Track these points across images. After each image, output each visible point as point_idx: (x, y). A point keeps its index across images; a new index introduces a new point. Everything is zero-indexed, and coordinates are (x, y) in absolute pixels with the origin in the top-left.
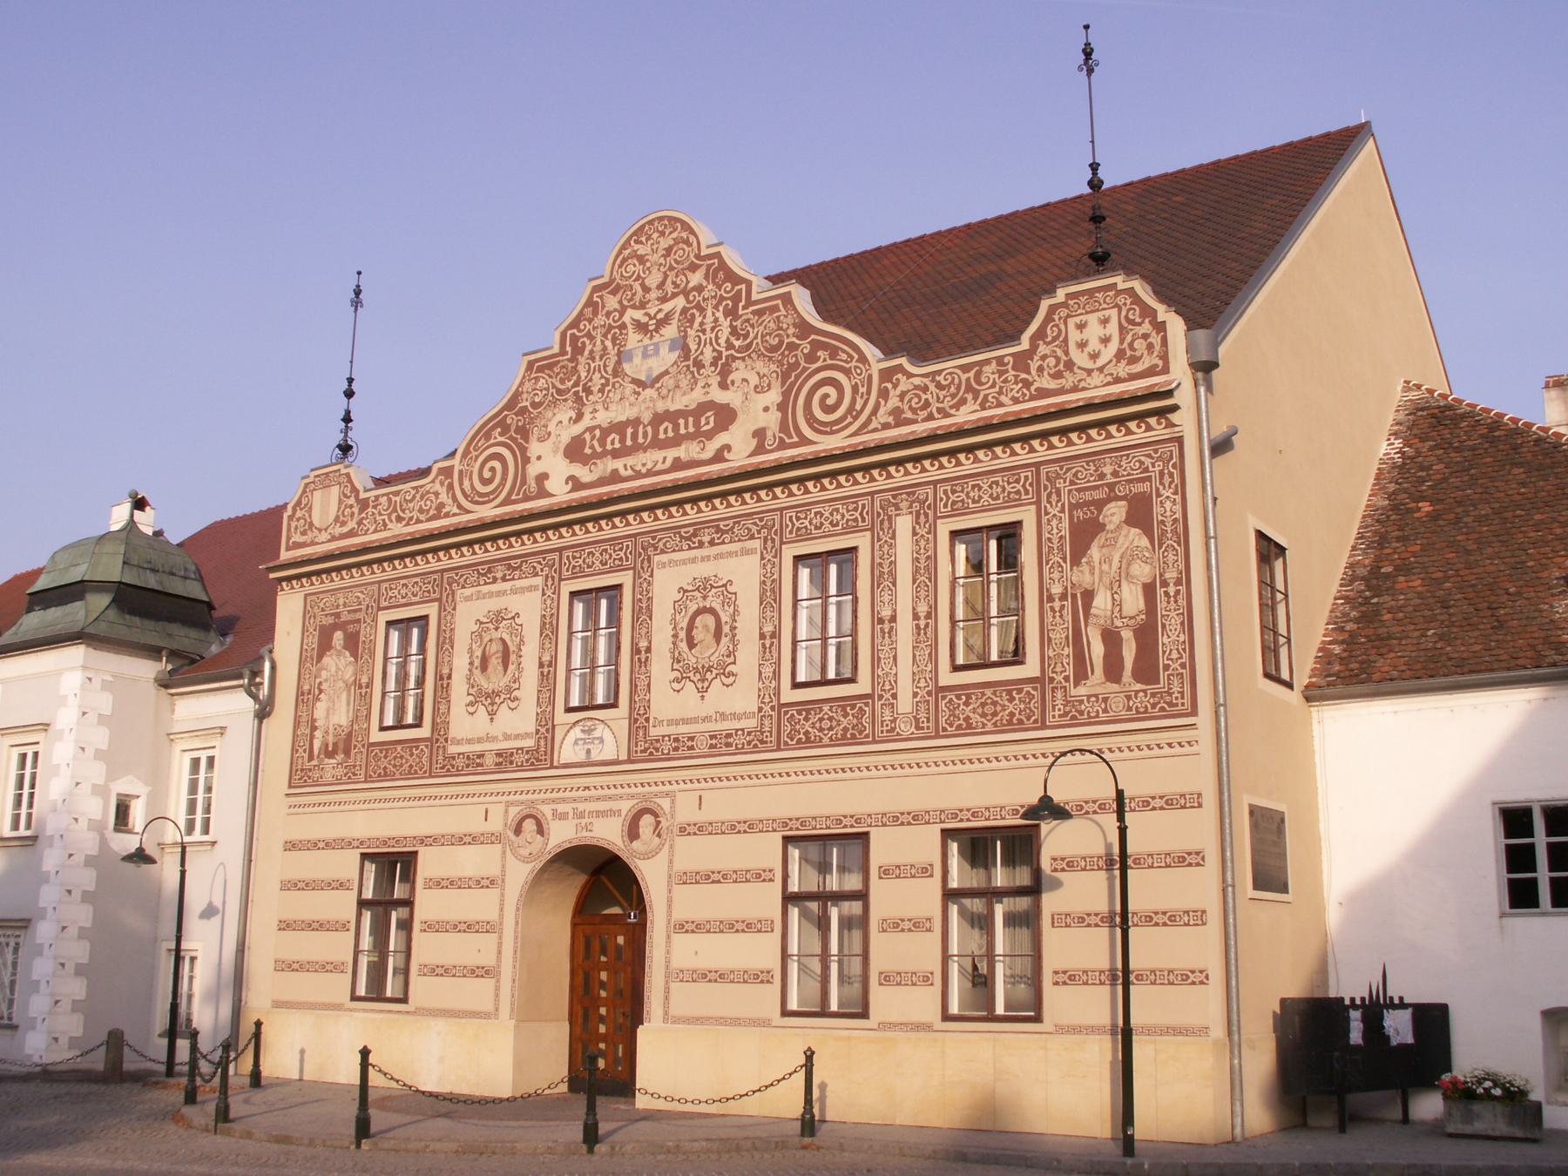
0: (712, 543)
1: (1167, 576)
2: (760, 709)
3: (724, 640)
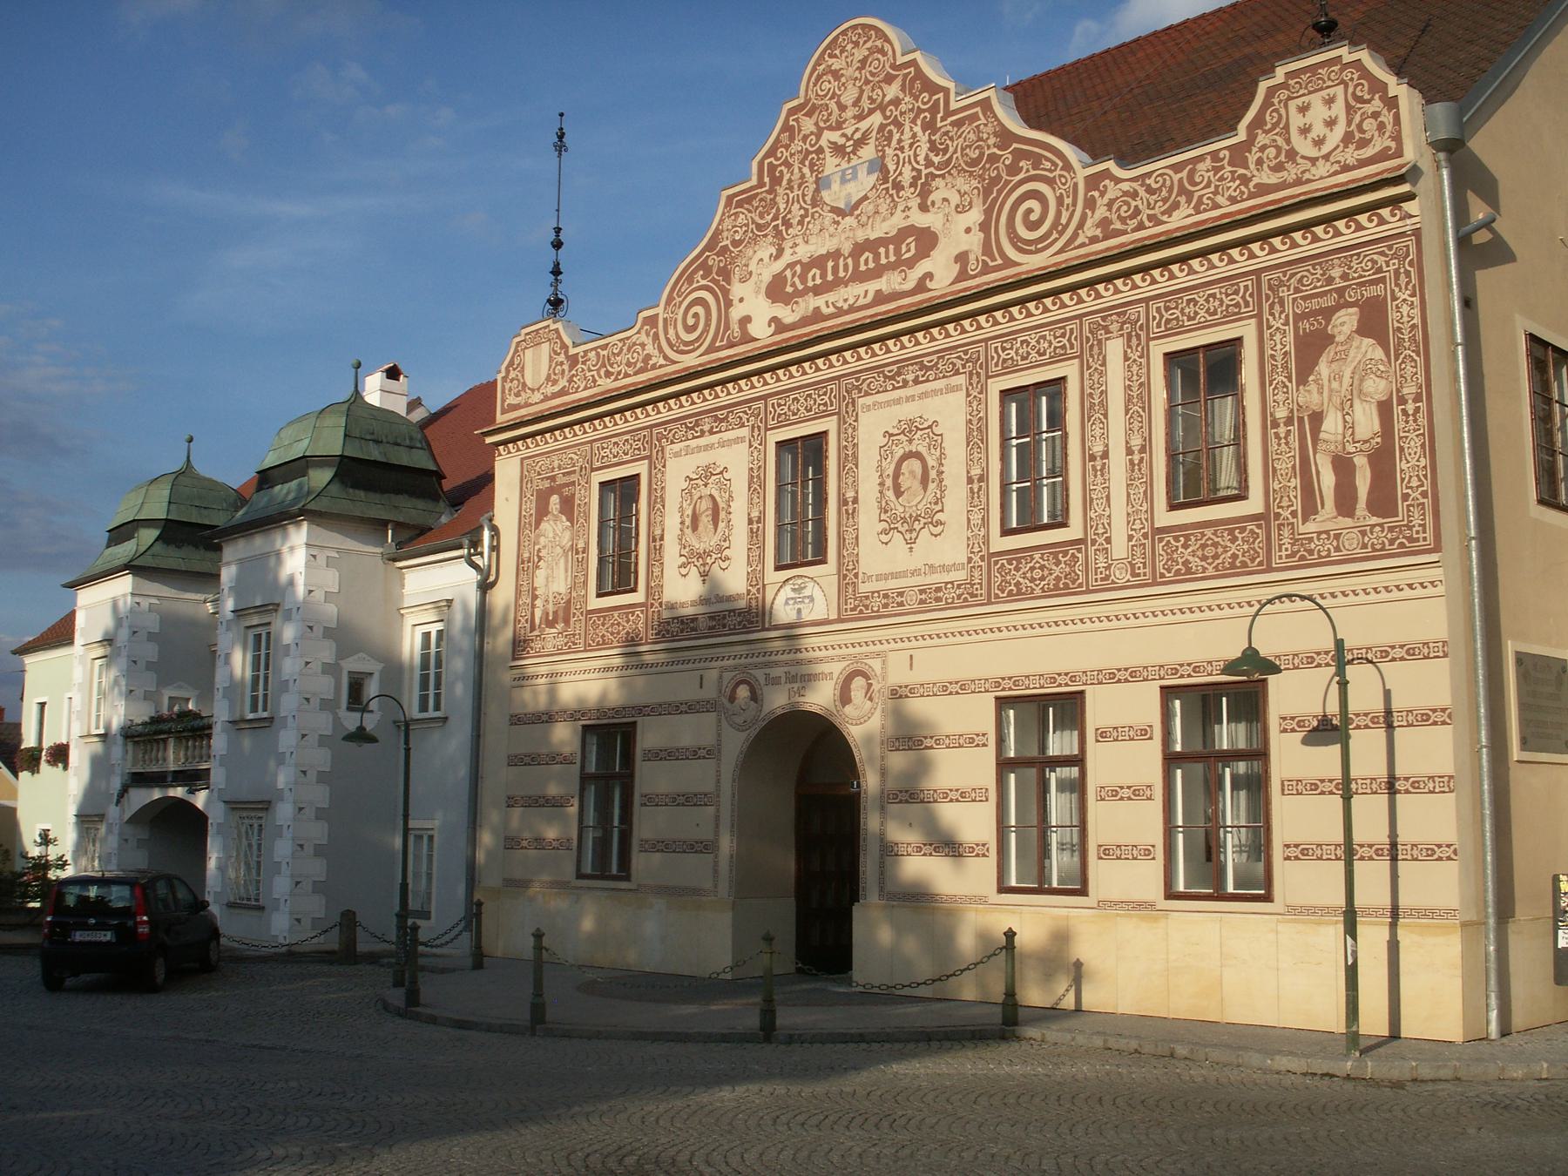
0: (916, 382)
1: (973, 473)
2: (970, 560)
3: (932, 486)
